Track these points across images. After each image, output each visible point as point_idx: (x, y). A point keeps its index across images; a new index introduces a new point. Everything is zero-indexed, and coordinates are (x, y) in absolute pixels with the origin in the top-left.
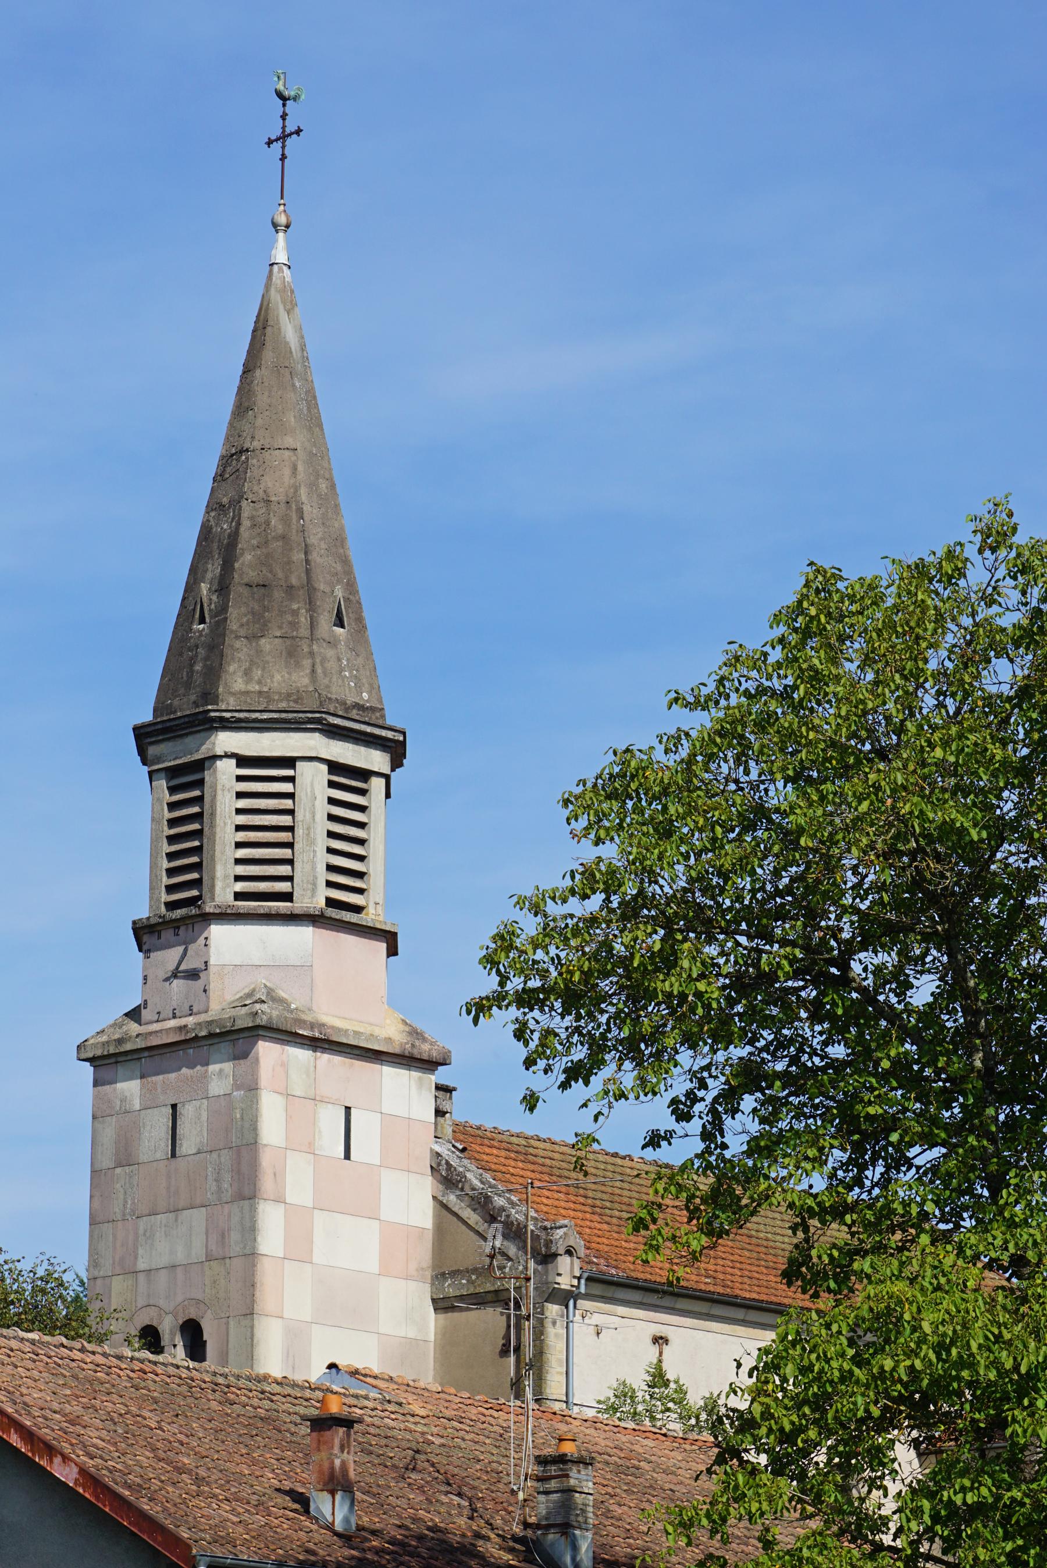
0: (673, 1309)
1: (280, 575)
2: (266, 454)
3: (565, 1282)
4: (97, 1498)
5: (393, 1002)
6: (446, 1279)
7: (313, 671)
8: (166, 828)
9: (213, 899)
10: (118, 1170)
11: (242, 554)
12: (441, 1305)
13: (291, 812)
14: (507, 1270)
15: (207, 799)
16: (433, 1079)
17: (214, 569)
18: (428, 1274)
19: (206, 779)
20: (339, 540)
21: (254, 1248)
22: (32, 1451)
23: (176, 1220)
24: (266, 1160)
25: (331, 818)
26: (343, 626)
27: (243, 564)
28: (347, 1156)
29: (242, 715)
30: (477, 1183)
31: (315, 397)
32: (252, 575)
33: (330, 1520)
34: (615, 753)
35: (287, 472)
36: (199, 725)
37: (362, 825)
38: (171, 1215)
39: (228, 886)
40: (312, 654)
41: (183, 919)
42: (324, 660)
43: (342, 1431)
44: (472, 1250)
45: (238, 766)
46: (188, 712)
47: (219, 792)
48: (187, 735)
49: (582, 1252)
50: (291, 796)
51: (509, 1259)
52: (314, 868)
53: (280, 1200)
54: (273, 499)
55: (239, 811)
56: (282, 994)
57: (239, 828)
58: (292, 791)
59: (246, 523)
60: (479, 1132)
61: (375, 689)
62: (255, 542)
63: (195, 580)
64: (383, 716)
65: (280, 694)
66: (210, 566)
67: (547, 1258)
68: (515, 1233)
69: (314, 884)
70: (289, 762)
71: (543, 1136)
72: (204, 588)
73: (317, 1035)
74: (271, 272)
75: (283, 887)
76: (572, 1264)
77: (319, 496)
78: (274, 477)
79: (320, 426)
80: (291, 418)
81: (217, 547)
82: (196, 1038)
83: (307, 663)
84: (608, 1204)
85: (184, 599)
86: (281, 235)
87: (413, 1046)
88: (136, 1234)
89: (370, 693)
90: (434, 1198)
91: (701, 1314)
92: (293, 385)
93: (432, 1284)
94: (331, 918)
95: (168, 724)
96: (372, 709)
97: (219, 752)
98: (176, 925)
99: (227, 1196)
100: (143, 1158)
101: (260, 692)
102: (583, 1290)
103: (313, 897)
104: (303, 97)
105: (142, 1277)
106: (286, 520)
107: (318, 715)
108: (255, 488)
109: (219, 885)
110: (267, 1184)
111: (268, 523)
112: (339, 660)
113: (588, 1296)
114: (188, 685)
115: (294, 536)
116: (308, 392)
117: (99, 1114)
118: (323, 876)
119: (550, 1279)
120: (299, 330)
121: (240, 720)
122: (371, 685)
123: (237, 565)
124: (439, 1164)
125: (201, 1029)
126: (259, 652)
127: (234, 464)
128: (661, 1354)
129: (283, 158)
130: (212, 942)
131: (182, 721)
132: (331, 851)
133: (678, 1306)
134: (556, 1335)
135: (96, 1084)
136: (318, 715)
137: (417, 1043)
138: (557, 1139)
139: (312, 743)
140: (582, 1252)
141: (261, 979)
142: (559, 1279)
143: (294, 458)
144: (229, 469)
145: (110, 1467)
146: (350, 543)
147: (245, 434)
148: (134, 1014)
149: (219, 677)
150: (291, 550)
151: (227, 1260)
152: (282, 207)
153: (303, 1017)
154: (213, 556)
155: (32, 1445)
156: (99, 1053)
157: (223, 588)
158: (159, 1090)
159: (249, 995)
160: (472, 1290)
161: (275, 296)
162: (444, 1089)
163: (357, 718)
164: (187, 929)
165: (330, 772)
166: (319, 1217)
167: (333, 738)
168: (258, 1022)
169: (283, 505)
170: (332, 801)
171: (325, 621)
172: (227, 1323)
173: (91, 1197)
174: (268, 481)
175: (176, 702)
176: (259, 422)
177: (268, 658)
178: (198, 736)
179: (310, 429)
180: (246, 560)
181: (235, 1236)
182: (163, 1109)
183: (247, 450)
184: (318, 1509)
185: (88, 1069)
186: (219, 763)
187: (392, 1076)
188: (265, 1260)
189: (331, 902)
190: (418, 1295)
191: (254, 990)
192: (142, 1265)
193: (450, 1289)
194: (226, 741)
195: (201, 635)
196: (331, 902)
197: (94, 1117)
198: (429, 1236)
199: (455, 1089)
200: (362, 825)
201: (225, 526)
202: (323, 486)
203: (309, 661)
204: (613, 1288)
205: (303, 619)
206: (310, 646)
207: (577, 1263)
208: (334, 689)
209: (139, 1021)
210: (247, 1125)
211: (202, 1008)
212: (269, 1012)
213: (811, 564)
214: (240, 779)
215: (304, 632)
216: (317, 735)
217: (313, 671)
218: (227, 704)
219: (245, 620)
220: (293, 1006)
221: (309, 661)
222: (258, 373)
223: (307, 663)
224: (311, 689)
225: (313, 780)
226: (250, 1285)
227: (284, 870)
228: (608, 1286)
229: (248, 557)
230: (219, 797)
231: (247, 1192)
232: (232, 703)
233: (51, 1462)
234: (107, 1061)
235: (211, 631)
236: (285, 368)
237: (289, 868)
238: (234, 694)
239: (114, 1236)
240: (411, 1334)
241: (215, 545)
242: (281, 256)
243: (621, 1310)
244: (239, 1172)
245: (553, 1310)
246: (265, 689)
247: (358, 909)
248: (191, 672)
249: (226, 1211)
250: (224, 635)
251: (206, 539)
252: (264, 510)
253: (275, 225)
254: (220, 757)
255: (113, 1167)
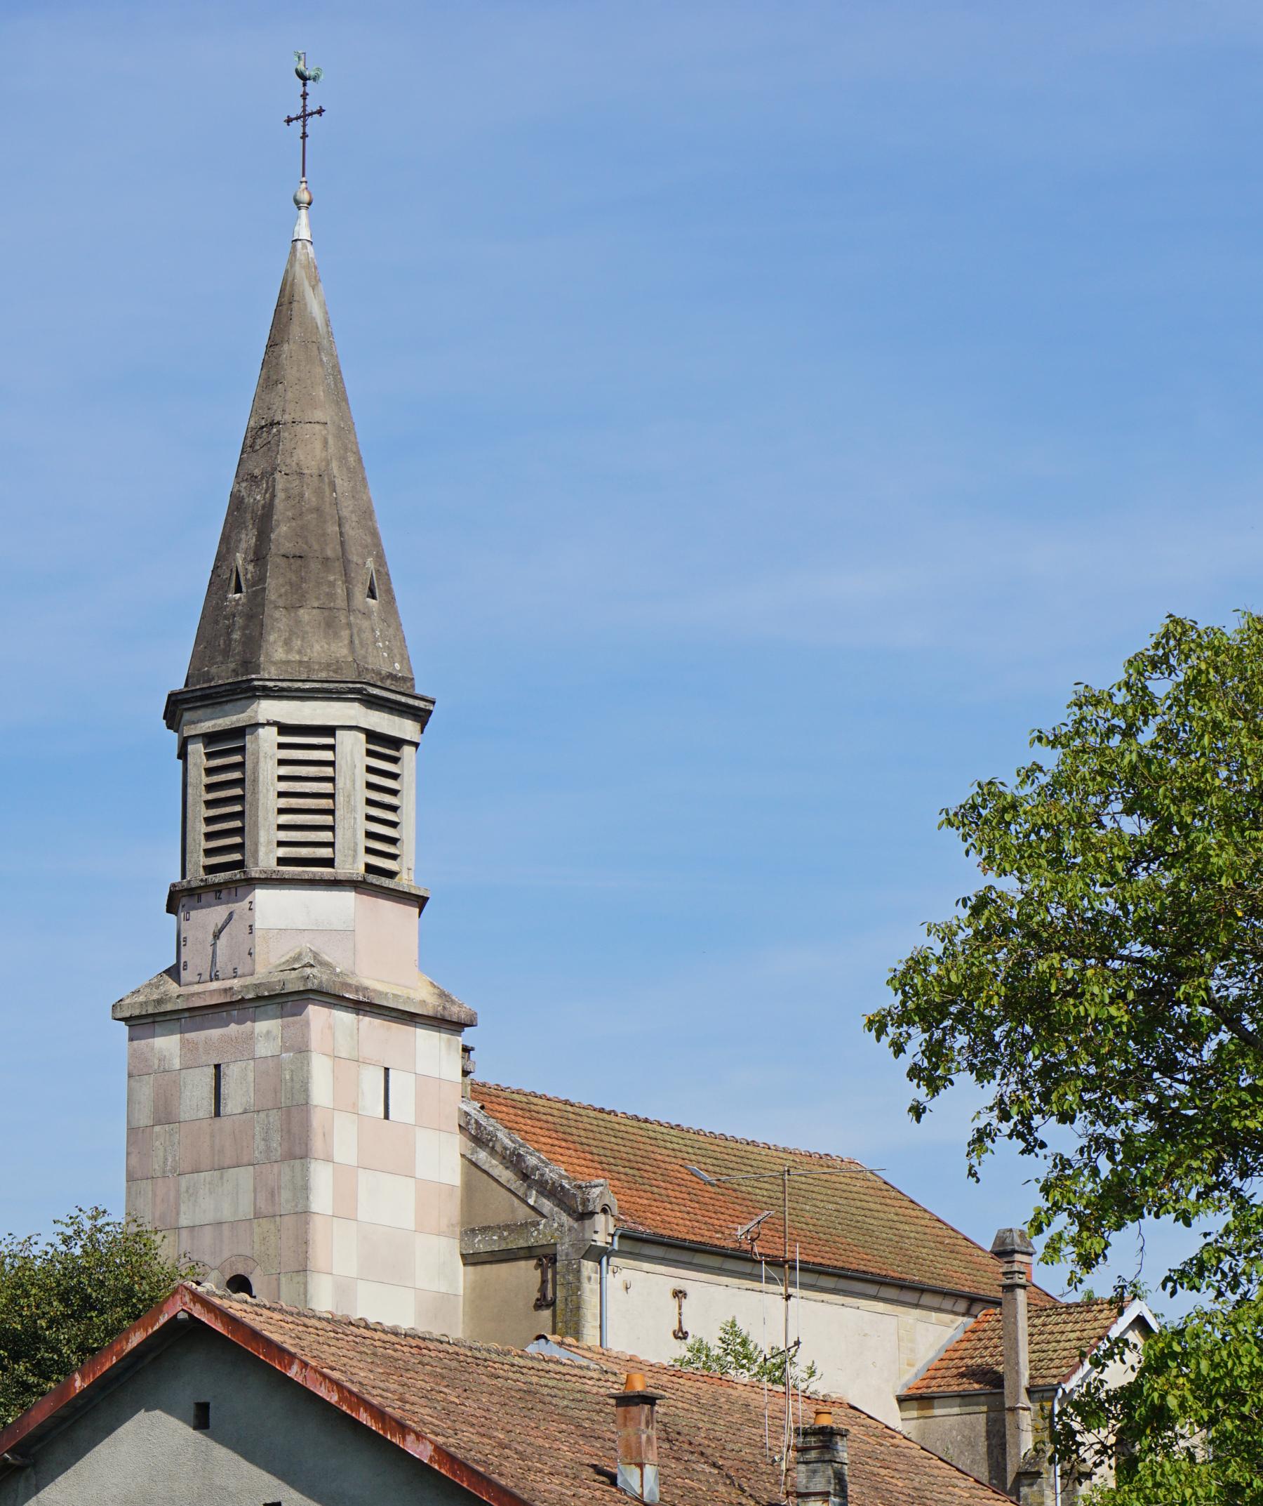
0: (690, 1263)
1: (316, 547)
2: (298, 428)
3: (601, 1240)
4: (454, 1474)
5: (424, 965)
6: (475, 1235)
7: (352, 642)
8: (203, 792)
9: (256, 864)
10: (157, 1128)
11: (278, 526)
12: (470, 1260)
13: (331, 780)
14: (541, 1227)
15: (248, 765)
16: (460, 1040)
17: (248, 539)
18: (458, 1230)
19: (248, 746)
20: (367, 513)
21: (307, 1206)
22: (383, 1429)
23: (222, 1178)
24: (317, 1120)
25: (370, 786)
26: (374, 597)
27: (279, 535)
28: (387, 1117)
29: (285, 685)
30: (507, 1142)
31: (340, 372)
32: (288, 547)
33: (639, 1492)
34: (980, 786)
35: (318, 445)
36: (241, 693)
37: (394, 792)
38: (217, 1173)
39: (271, 851)
40: (349, 625)
41: (226, 884)
42: (360, 630)
43: (647, 1407)
44: (503, 1208)
45: (280, 733)
46: (230, 680)
47: (262, 759)
48: (227, 702)
49: (616, 1211)
50: (331, 764)
51: (544, 1216)
52: (354, 835)
53: (329, 1159)
54: (305, 471)
55: (281, 778)
56: (327, 958)
57: (281, 795)
58: (332, 758)
59: (280, 495)
60: (485, 1090)
61: (405, 659)
62: (290, 514)
63: (228, 549)
64: (413, 686)
65: (320, 663)
66: (243, 536)
67: (585, 1216)
68: (550, 1192)
69: (355, 851)
70: (330, 731)
71: (539, 1093)
72: (239, 557)
73: (361, 998)
74: (294, 249)
75: (325, 852)
76: (607, 1221)
77: (349, 469)
78: (308, 450)
79: (346, 400)
80: (320, 393)
81: (250, 517)
82: (243, 1000)
83: (345, 634)
84: (612, 1160)
85: (216, 568)
86: (303, 212)
87: (444, 1008)
88: (178, 1191)
89: (401, 663)
90: (463, 1156)
91: (713, 1268)
92: (321, 360)
93: (462, 1240)
94: (372, 884)
95: (208, 692)
96: (404, 679)
97: (262, 721)
98: (217, 889)
99: (277, 1155)
100: (183, 1117)
101: (300, 662)
102: (616, 1247)
103: (352, 863)
104: (322, 77)
105: (184, 1233)
106: (319, 492)
107: (358, 686)
108: (288, 461)
109: (262, 850)
110: (317, 1144)
111: (302, 495)
112: (373, 630)
113: (620, 1254)
114: (226, 653)
115: (327, 509)
116: (333, 367)
117: (135, 1072)
118: (363, 842)
119: (587, 1236)
120: (323, 305)
121: (282, 689)
122: (402, 655)
123: (273, 536)
124: (468, 1123)
125: (248, 993)
126: (298, 622)
127: (263, 436)
128: (680, 1307)
129: (304, 136)
130: (257, 906)
131: (223, 688)
132: (369, 818)
133: (695, 1261)
134: (591, 1290)
135: (131, 1039)
136: (358, 686)
137: (448, 1005)
138: (550, 1095)
139: (352, 712)
140: (616, 1211)
141: (305, 944)
142: (596, 1237)
143: (324, 432)
144: (259, 441)
145: (468, 1442)
146: (378, 516)
147: (274, 407)
148: (174, 972)
149: (260, 647)
150: (325, 522)
151: (278, 1219)
152: (304, 185)
153: (350, 981)
154: (246, 527)
155: (384, 1423)
156: (136, 1012)
157: (259, 557)
158: (201, 1049)
159: (298, 958)
160: (503, 1246)
161: (300, 273)
162: (466, 1050)
163: (393, 687)
164: (229, 893)
165: (368, 742)
166: (363, 1175)
167: (370, 708)
168: (310, 986)
169: (316, 479)
170: (370, 769)
171: (360, 592)
172: (278, 1280)
173: (128, 1154)
174: (300, 454)
175: (214, 670)
176: (290, 395)
177: (308, 628)
178: (239, 703)
179: (338, 403)
180: (282, 532)
181: (285, 1195)
182: (205, 1069)
183: (278, 423)
184: (626, 1481)
185: (123, 1028)
186: (261, 730)
187: (425, 1038)
188: (316, 1218)
189: (370, 868)
190: (448, 1249)
191: (300, 954)
192: (184, 1221)
193: (481, 1244)
194: (268, 709)
195: (237, 604)
196: (370, 868)
197: (130, 1076)
198: (458, 1193)
199: (473, 1049)
200: (394, 792)
201: (258, 497)
202: (352, 459)
203: (348, 632)
204: (640, 1244)
205: (339, 591)
206: (348, 617)
207: (611, 1221)
208: (370, 660)
209: (177, 979)
210: (297, 1086)
211: (247, 970)
212: (319, 977)
213: (1170, 616)
214: (281, 746)
215: (341, 603)
216: (356, 705)
217: (352, 642)
218: (268, 673)
219: (283, 590)
220: (338, 970)
221: (348, 632)
222: (286, 347)
223: (345, 634)
224: (350, 659)
225: (351, 748)
226: (303, 1243)
227: (325, 836)
228: (640, 1244)
229: (284, 529)
230: (262, 764)
231: (298, 1151)
232: (273, 672)
233: (404, 1439)
234: (143, 1022)
235: (249, 600)
236: (315, 344)
237: (330, 834)
238: (274, 663)
239: (154, 1195)
240: (443, 1290)
241: (248, 516)
242: (303, 231)
243: (646, 1266)
244: (289, 1132)
245: (588, 1267)
246: (306, 659)
247: (391, 874)
248: (229, 640)
249: (276, 1170)
250: (264, 605)
251: (238, 509)
252: (297, 482)
253: (297, 202)
254: (263, 725)
255: (150, 1126)
